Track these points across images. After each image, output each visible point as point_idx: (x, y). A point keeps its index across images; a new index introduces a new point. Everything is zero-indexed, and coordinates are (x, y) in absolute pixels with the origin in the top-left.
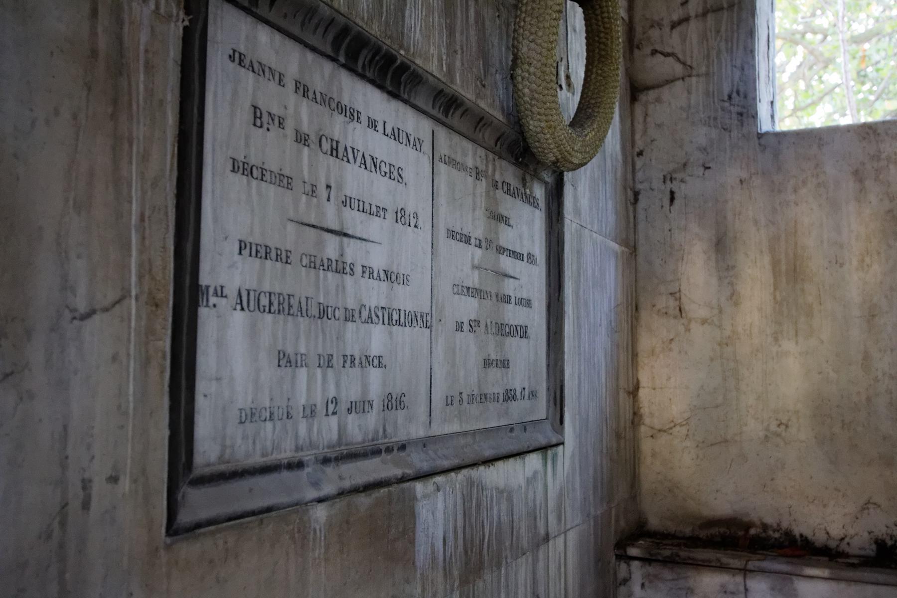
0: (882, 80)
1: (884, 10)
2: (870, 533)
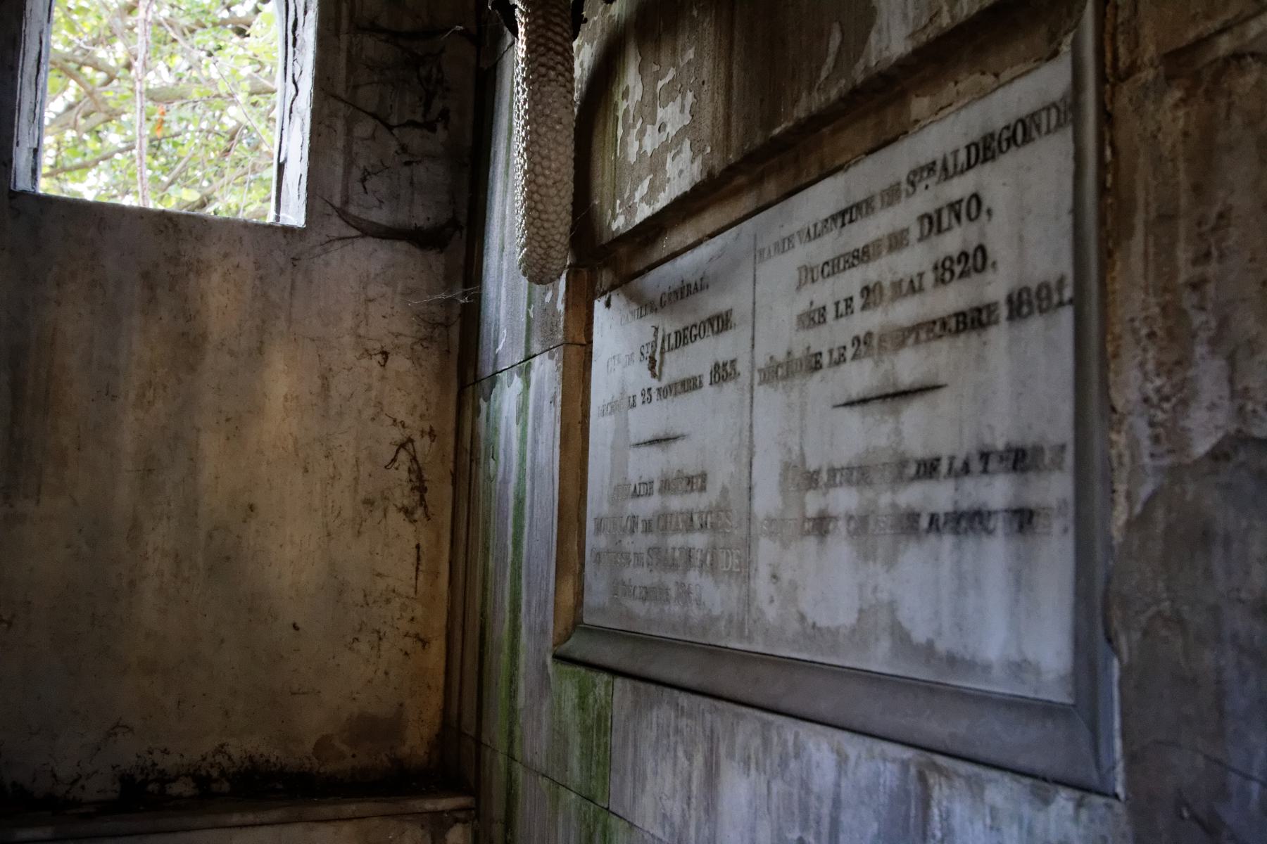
0: (180, 159)
1: (190, 68)
2: (114, 768)
